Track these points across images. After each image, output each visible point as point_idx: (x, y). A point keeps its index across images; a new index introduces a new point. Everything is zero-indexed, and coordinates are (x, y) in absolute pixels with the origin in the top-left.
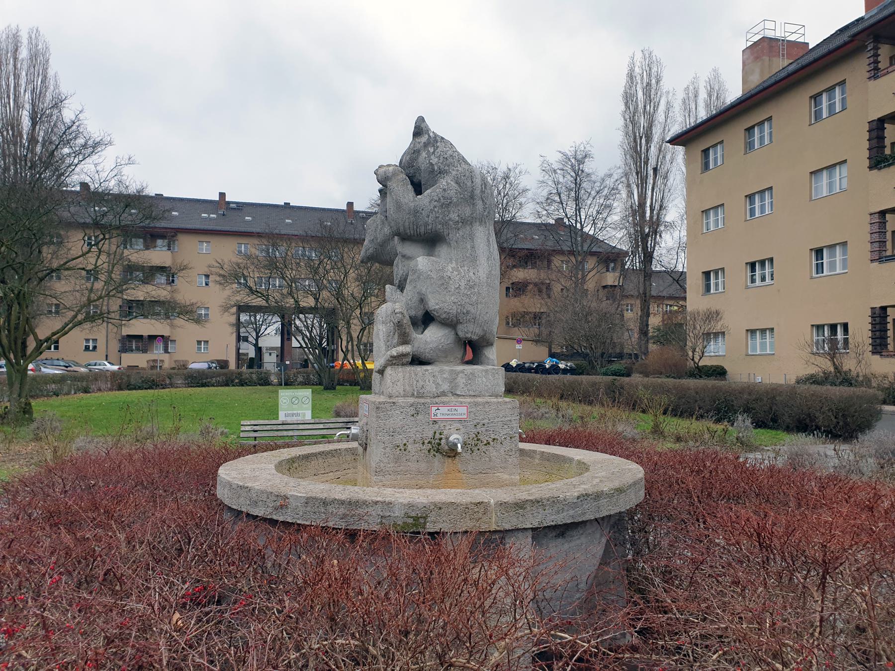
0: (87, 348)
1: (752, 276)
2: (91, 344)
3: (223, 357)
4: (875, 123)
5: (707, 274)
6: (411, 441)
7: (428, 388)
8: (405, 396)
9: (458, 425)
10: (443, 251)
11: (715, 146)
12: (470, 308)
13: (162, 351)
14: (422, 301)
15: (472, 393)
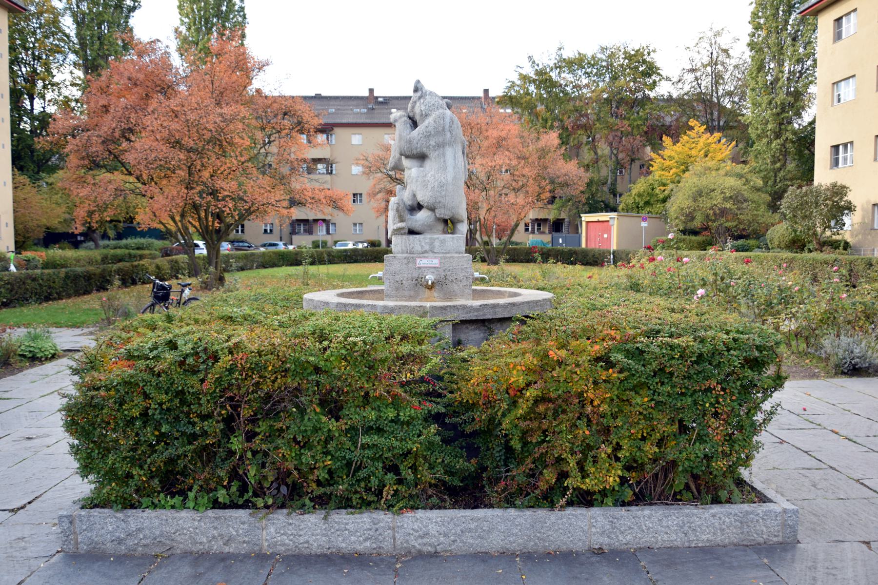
0: (266, 231)
2: (268, 228)
3: (373, 238)
5: (836, 148)
6: (405, 279)
7: (416, 248)
8: (402, 253)
9: (433, 270)
11: (848, 14)
12: (441, 199)
13: (325, 233)
14: (414, 196)
15: (444, 251)
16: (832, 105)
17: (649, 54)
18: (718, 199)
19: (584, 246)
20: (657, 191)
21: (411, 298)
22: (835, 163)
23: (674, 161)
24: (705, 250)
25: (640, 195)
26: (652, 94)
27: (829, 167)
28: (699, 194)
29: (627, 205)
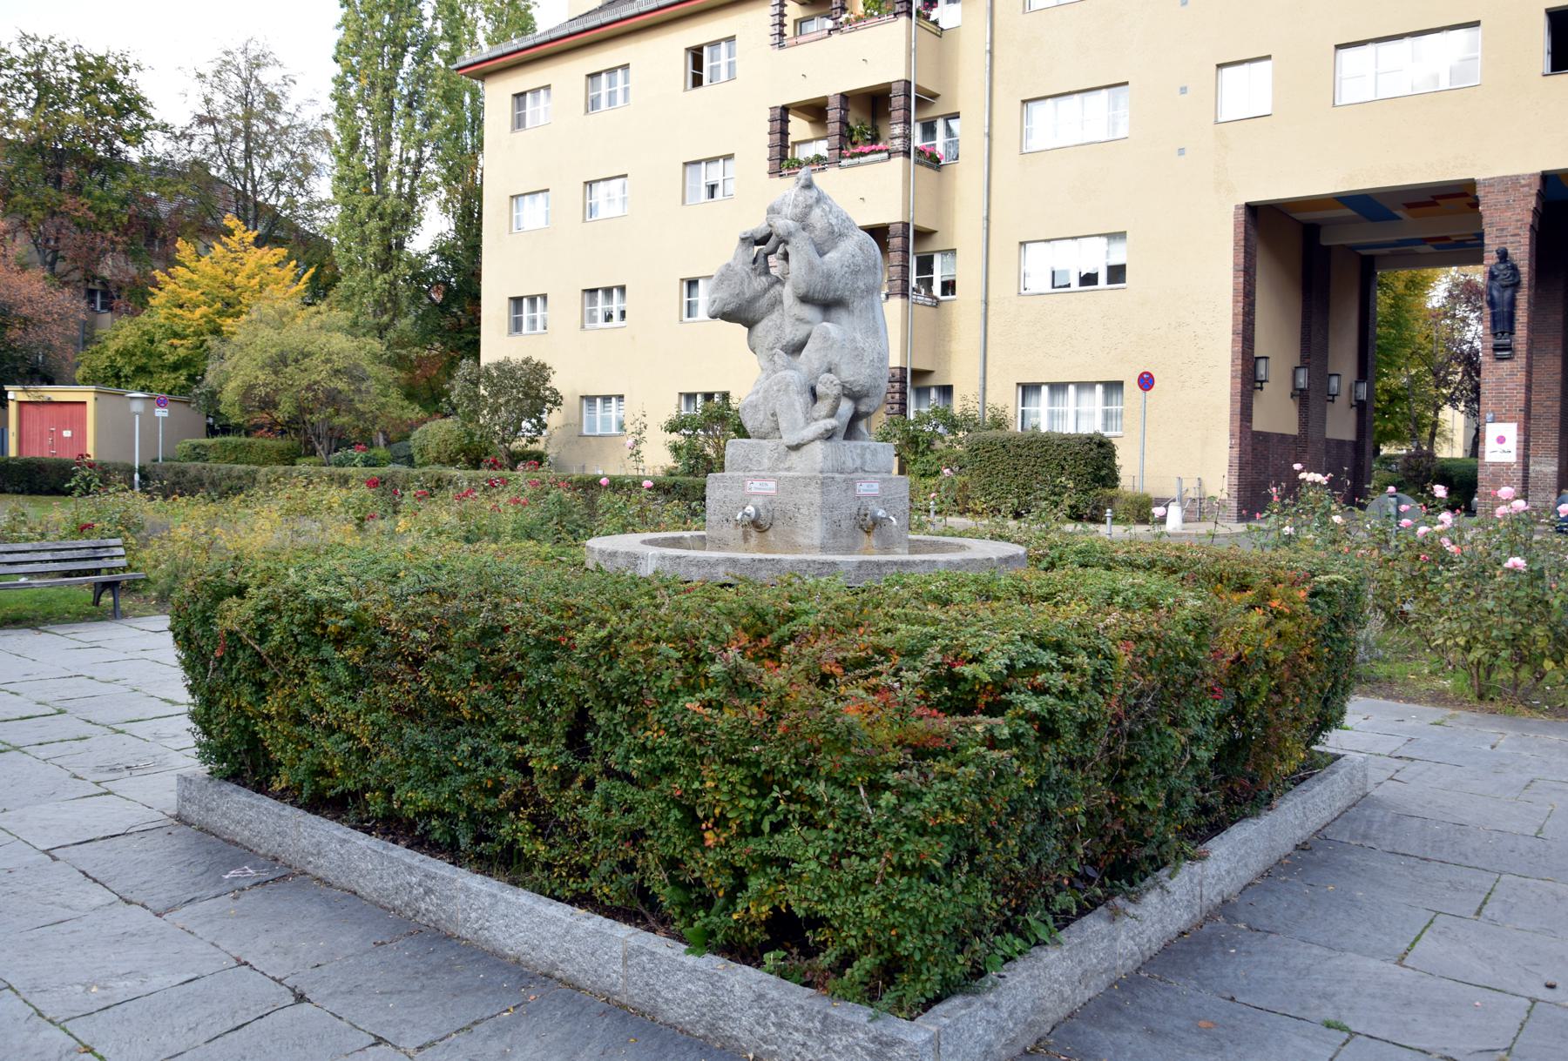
1: (591, 311)
4: (778, 111)
5: (517, 302)
10: (841, 315)
16: (511, 232)
17: (126, 72)
18: (320, 374)
19: (12, 452)
20: (163, 348)
21: (849, 550)
22: (517, 326)
23: (200, 291)
24: (293, 464)
25: (126, 353)
26: (134, 154)
27: (506, 331)
28: (279, 362)
29: (94, 371)
